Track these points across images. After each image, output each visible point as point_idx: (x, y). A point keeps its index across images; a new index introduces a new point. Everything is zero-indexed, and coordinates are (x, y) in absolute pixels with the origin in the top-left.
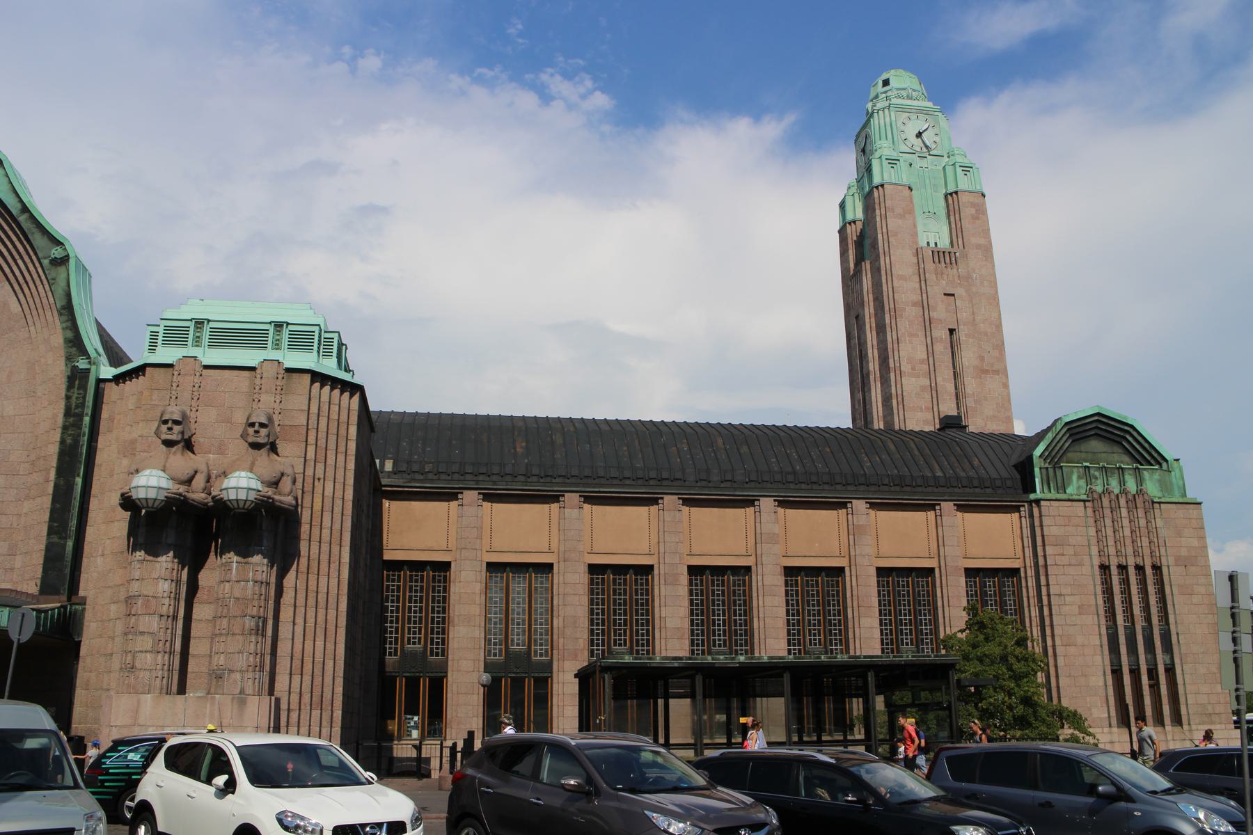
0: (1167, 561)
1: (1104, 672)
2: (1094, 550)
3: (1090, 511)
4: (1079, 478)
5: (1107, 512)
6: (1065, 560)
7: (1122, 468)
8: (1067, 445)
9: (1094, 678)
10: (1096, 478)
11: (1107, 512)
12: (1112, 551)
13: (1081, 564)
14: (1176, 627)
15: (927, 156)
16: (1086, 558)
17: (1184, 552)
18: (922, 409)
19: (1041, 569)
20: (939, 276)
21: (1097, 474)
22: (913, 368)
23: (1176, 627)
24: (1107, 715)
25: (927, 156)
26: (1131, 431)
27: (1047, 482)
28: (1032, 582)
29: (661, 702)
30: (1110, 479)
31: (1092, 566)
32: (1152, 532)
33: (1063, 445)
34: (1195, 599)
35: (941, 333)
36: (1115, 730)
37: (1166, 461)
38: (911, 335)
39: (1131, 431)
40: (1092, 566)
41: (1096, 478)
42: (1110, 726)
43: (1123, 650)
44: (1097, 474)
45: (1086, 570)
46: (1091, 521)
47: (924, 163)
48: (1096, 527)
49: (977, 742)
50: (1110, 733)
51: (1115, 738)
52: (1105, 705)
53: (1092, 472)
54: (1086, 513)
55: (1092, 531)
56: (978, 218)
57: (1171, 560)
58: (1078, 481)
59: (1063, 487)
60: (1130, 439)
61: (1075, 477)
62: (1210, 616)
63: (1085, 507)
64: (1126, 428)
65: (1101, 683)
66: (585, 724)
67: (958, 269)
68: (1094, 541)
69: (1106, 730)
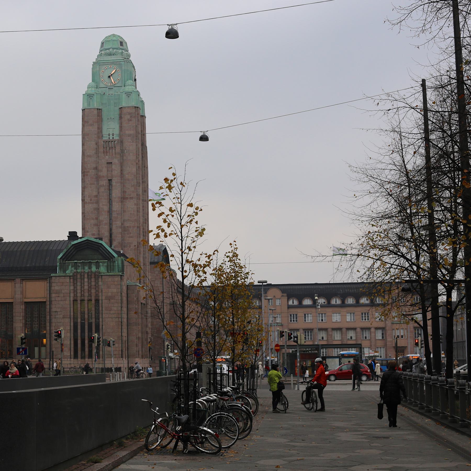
0: (102, 297)
1: (70, 339)
2: (72, 295)
3: (72, 280)
4: (72, 267)
5: (79, 280)
6: (59, 299)
7: (91, 262)
8: (75, 253)
9: (66, 341)
10: (79, 266)
11: (79, 280)
12: (79, 295)
13: (65, 300)
14: (102, 323)
15: (113, 87)
16: (68, 298)
17: (110, 294)
18: (93, 218)
19: (51, 302)
20: (105, 154)
21: (80, 265)
22: (91, 200)
23: (102, 323)
24: (69, 354)
25: (113, 87)
26: (101, 246)
27: (60, 269)
28: (48, 307)
29: (36, 349)
30: (85, 267)
31: (70, 301)
32: (97, 286)
33: (73, 252)
34: (112, 312)
35: (104, 182)
36: (72, 359)
37: (114, 257)
38: (91, 184)
39: (101, 246)
40: (70, 301)
41: (79, 266)
42: (71, 358)
43: (79, 331)
44: (80, 265)
45: (67, 302)
46: (72, 284)
47: (111, 92)
48: (74, 286)
49: (6, 362)
50: (70, 361)
51: (72, 362)
52: (69, 351)
53: (78, 264)
54: (70, 281)
55: (72, 288)
56: (131, 120)
57: (104, 298)
58: (71, 268)
59: (65, 271)
60: (101, 249)
61: (70, 267)
62: (117, 319)
63: (70, 279)
64: (99, 245)
65: (69, 343)
66: (351, 379)
67: (115, 150)
68: (72, 291)
69: (69, 359)
